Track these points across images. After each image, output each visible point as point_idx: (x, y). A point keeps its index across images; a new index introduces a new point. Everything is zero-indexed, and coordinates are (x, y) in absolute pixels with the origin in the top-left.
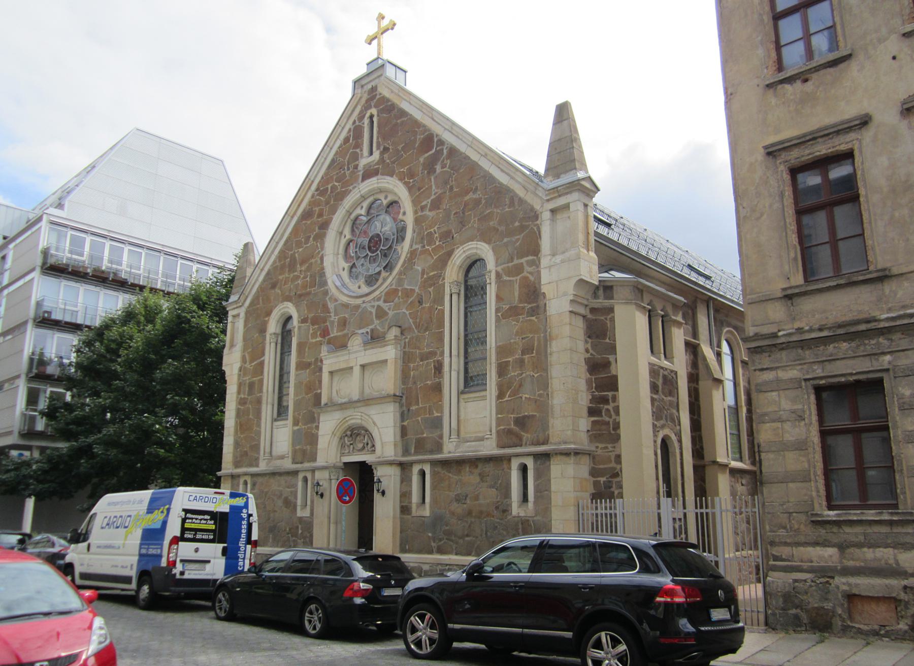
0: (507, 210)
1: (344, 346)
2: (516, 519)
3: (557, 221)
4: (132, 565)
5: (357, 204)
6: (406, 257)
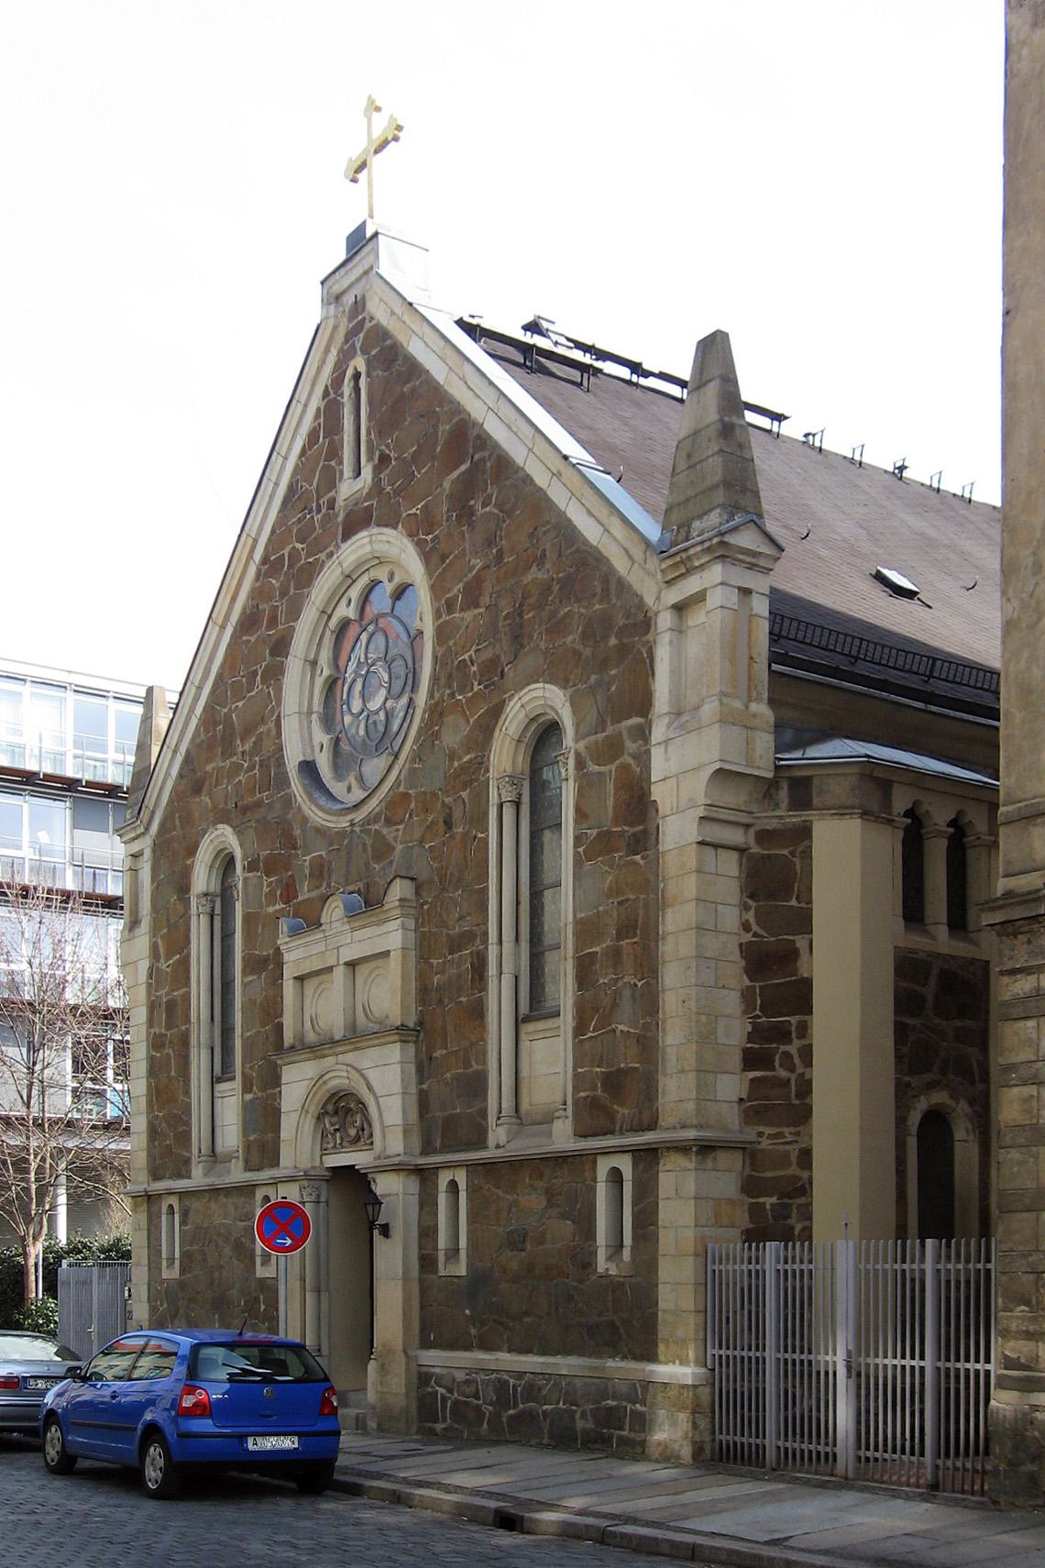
0: (597, 607)
1: (317, 924)
2: (603, 1281)
3: (689, 632)
5: (337, 595)
6: (422, 719)
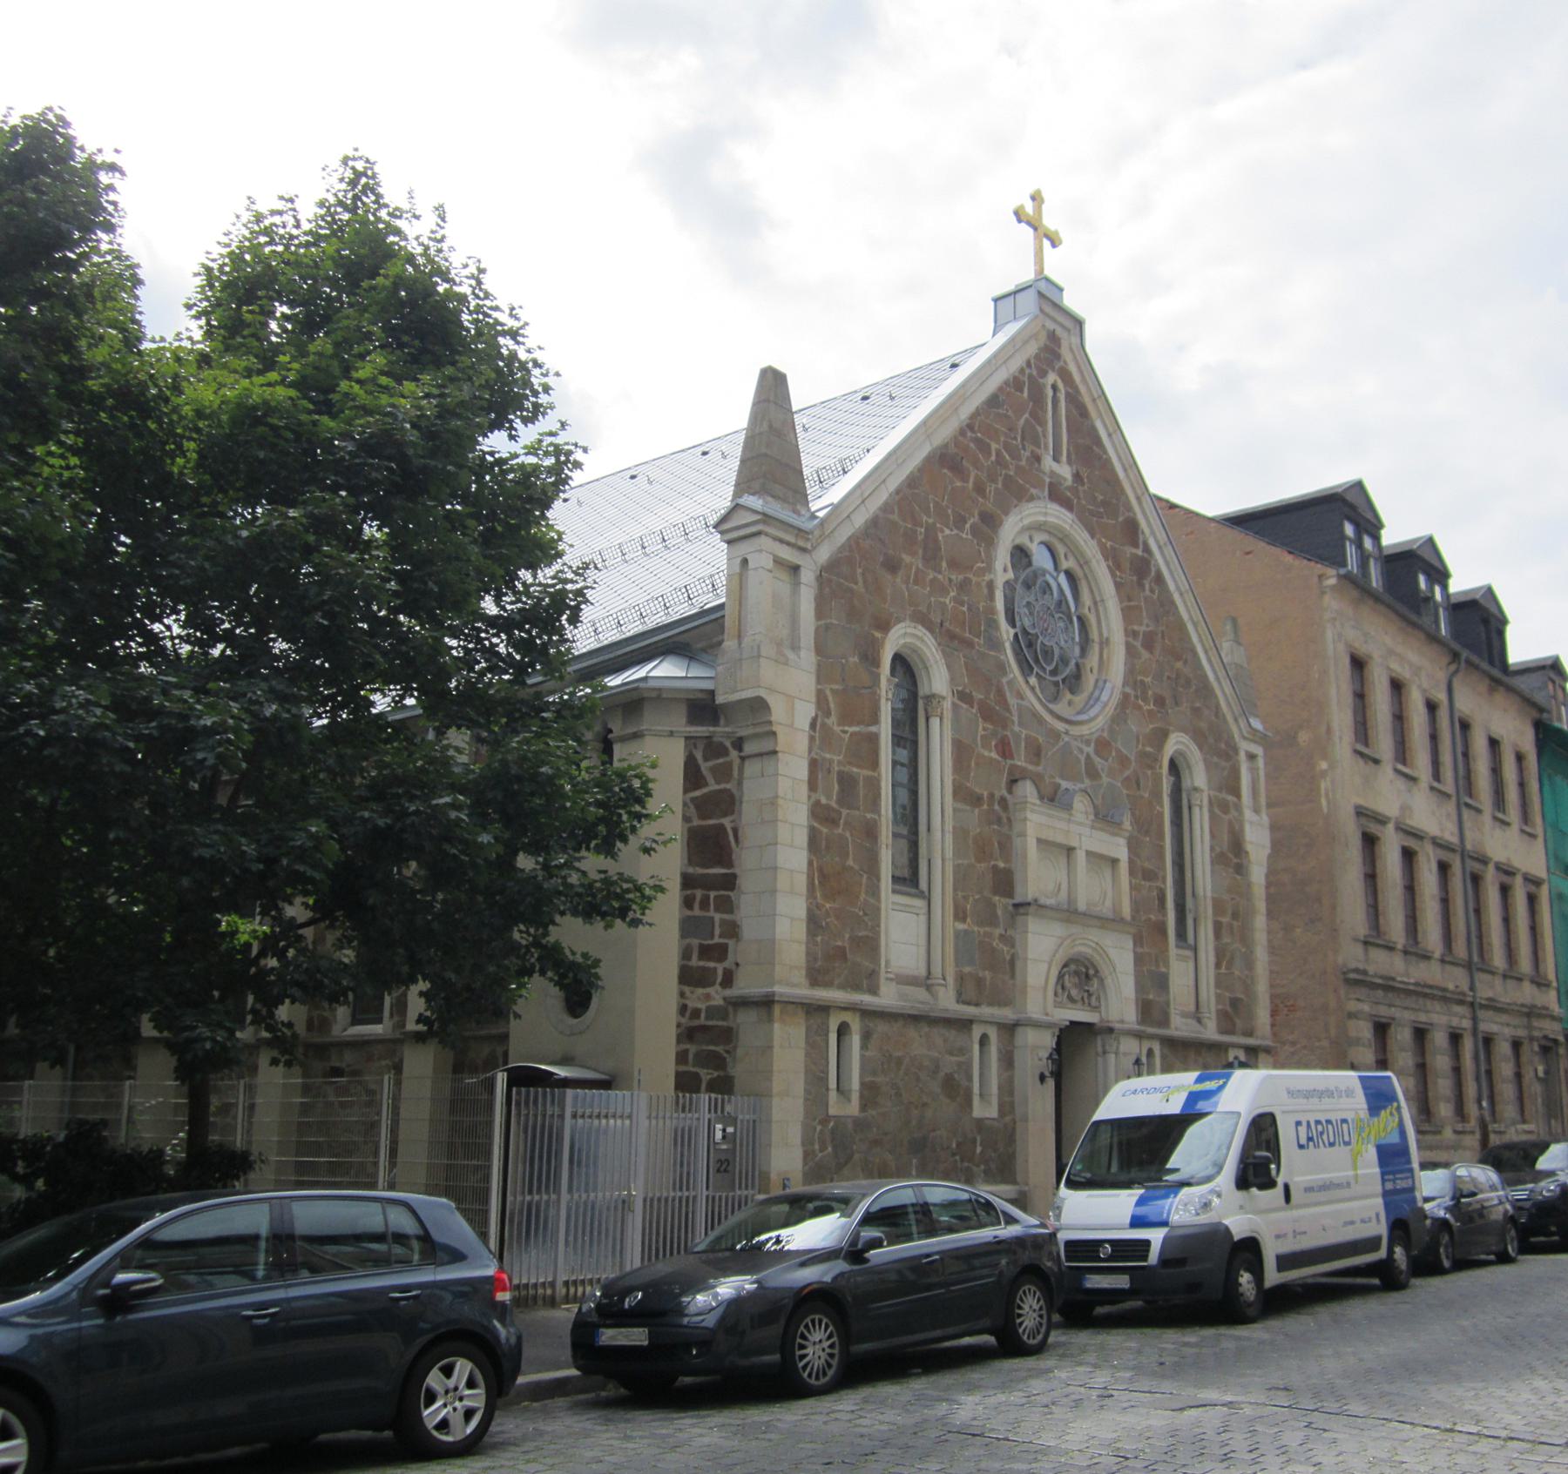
4: (1377, 1215)
